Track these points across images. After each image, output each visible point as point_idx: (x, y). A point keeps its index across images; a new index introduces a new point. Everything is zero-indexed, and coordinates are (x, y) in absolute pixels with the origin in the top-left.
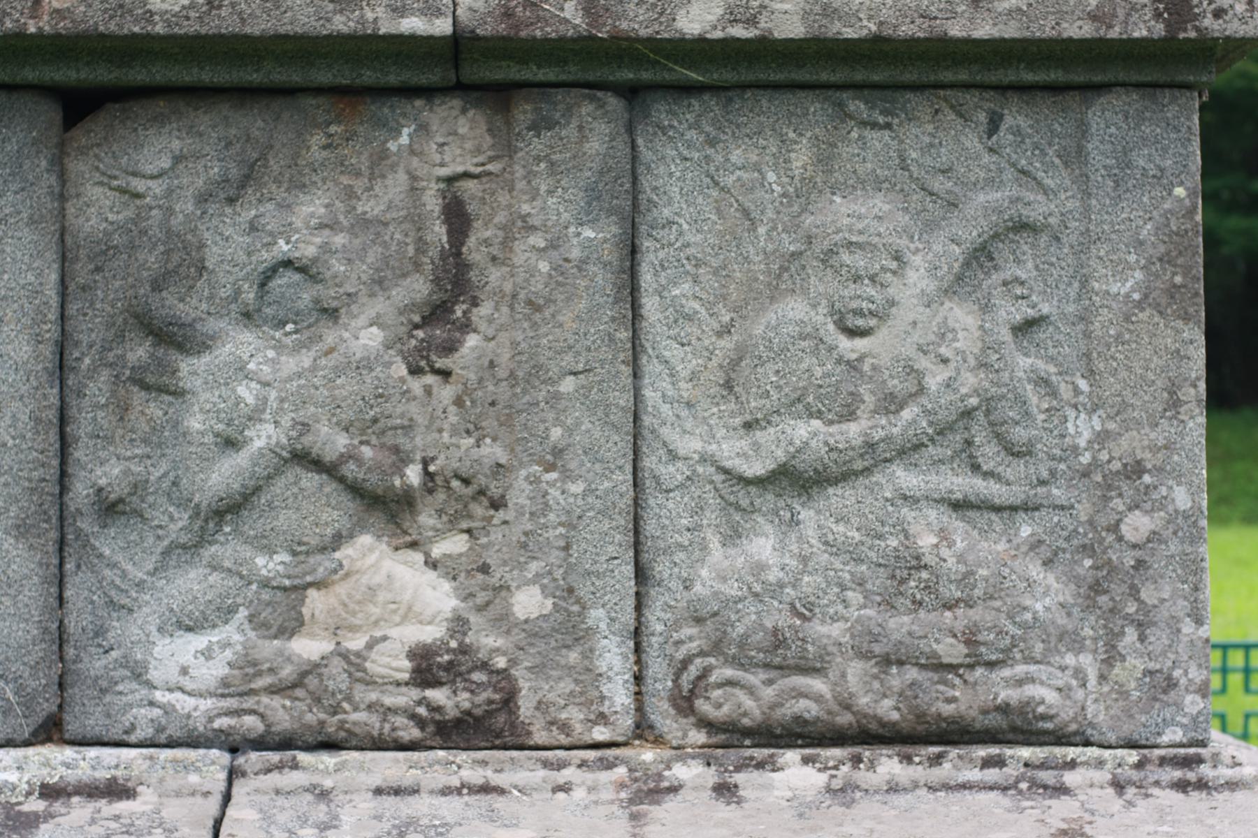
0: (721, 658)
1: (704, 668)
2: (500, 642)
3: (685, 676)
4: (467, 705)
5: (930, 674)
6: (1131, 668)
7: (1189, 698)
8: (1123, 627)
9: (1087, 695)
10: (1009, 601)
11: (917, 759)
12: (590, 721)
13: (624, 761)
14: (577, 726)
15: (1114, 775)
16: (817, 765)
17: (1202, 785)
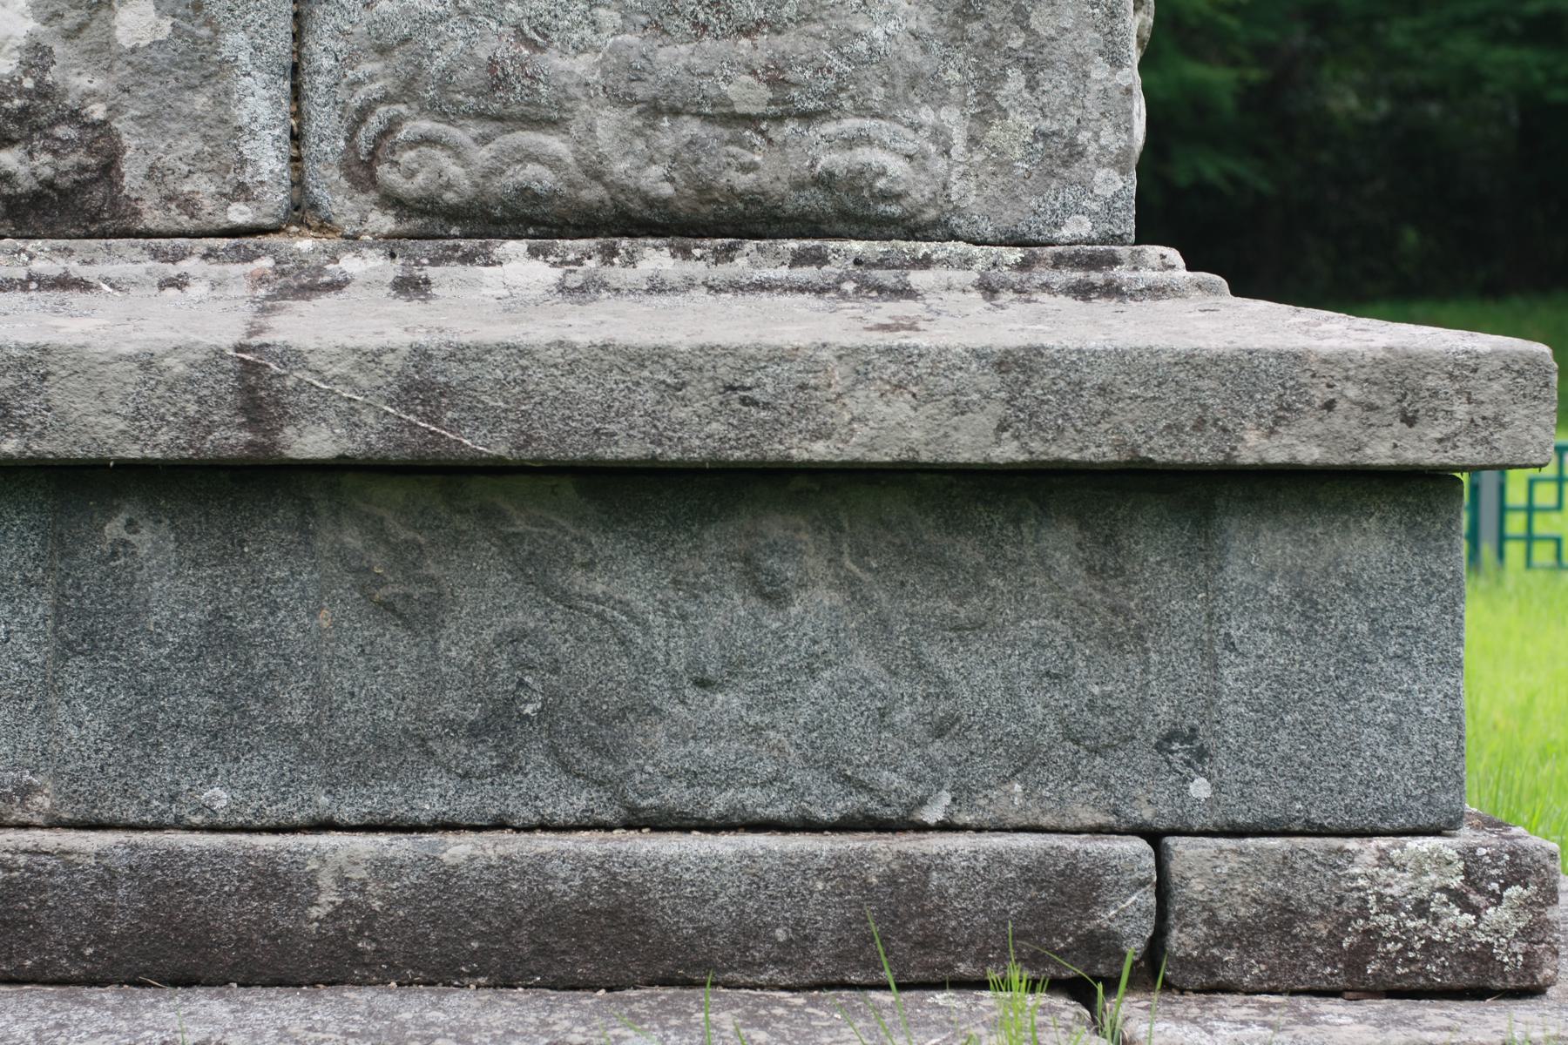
0: (415, 105)
1: (390, 120)
2: (98, 83)
3: (362, 133)
4: (47, 172)
5: (719, 130)
6: (1018, 125)
7: (1101, 174)
8: (1003, 68)
9: (950, 167)
10: (833, 23)
11: (697, 252)
12: (224, 195)
13: (270, 251)
14: (206, 202)
15: (983, 276)
16: (551, 258)
17: (1112, 290)
